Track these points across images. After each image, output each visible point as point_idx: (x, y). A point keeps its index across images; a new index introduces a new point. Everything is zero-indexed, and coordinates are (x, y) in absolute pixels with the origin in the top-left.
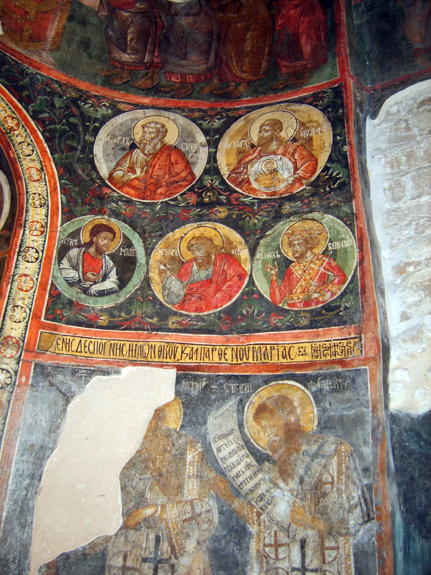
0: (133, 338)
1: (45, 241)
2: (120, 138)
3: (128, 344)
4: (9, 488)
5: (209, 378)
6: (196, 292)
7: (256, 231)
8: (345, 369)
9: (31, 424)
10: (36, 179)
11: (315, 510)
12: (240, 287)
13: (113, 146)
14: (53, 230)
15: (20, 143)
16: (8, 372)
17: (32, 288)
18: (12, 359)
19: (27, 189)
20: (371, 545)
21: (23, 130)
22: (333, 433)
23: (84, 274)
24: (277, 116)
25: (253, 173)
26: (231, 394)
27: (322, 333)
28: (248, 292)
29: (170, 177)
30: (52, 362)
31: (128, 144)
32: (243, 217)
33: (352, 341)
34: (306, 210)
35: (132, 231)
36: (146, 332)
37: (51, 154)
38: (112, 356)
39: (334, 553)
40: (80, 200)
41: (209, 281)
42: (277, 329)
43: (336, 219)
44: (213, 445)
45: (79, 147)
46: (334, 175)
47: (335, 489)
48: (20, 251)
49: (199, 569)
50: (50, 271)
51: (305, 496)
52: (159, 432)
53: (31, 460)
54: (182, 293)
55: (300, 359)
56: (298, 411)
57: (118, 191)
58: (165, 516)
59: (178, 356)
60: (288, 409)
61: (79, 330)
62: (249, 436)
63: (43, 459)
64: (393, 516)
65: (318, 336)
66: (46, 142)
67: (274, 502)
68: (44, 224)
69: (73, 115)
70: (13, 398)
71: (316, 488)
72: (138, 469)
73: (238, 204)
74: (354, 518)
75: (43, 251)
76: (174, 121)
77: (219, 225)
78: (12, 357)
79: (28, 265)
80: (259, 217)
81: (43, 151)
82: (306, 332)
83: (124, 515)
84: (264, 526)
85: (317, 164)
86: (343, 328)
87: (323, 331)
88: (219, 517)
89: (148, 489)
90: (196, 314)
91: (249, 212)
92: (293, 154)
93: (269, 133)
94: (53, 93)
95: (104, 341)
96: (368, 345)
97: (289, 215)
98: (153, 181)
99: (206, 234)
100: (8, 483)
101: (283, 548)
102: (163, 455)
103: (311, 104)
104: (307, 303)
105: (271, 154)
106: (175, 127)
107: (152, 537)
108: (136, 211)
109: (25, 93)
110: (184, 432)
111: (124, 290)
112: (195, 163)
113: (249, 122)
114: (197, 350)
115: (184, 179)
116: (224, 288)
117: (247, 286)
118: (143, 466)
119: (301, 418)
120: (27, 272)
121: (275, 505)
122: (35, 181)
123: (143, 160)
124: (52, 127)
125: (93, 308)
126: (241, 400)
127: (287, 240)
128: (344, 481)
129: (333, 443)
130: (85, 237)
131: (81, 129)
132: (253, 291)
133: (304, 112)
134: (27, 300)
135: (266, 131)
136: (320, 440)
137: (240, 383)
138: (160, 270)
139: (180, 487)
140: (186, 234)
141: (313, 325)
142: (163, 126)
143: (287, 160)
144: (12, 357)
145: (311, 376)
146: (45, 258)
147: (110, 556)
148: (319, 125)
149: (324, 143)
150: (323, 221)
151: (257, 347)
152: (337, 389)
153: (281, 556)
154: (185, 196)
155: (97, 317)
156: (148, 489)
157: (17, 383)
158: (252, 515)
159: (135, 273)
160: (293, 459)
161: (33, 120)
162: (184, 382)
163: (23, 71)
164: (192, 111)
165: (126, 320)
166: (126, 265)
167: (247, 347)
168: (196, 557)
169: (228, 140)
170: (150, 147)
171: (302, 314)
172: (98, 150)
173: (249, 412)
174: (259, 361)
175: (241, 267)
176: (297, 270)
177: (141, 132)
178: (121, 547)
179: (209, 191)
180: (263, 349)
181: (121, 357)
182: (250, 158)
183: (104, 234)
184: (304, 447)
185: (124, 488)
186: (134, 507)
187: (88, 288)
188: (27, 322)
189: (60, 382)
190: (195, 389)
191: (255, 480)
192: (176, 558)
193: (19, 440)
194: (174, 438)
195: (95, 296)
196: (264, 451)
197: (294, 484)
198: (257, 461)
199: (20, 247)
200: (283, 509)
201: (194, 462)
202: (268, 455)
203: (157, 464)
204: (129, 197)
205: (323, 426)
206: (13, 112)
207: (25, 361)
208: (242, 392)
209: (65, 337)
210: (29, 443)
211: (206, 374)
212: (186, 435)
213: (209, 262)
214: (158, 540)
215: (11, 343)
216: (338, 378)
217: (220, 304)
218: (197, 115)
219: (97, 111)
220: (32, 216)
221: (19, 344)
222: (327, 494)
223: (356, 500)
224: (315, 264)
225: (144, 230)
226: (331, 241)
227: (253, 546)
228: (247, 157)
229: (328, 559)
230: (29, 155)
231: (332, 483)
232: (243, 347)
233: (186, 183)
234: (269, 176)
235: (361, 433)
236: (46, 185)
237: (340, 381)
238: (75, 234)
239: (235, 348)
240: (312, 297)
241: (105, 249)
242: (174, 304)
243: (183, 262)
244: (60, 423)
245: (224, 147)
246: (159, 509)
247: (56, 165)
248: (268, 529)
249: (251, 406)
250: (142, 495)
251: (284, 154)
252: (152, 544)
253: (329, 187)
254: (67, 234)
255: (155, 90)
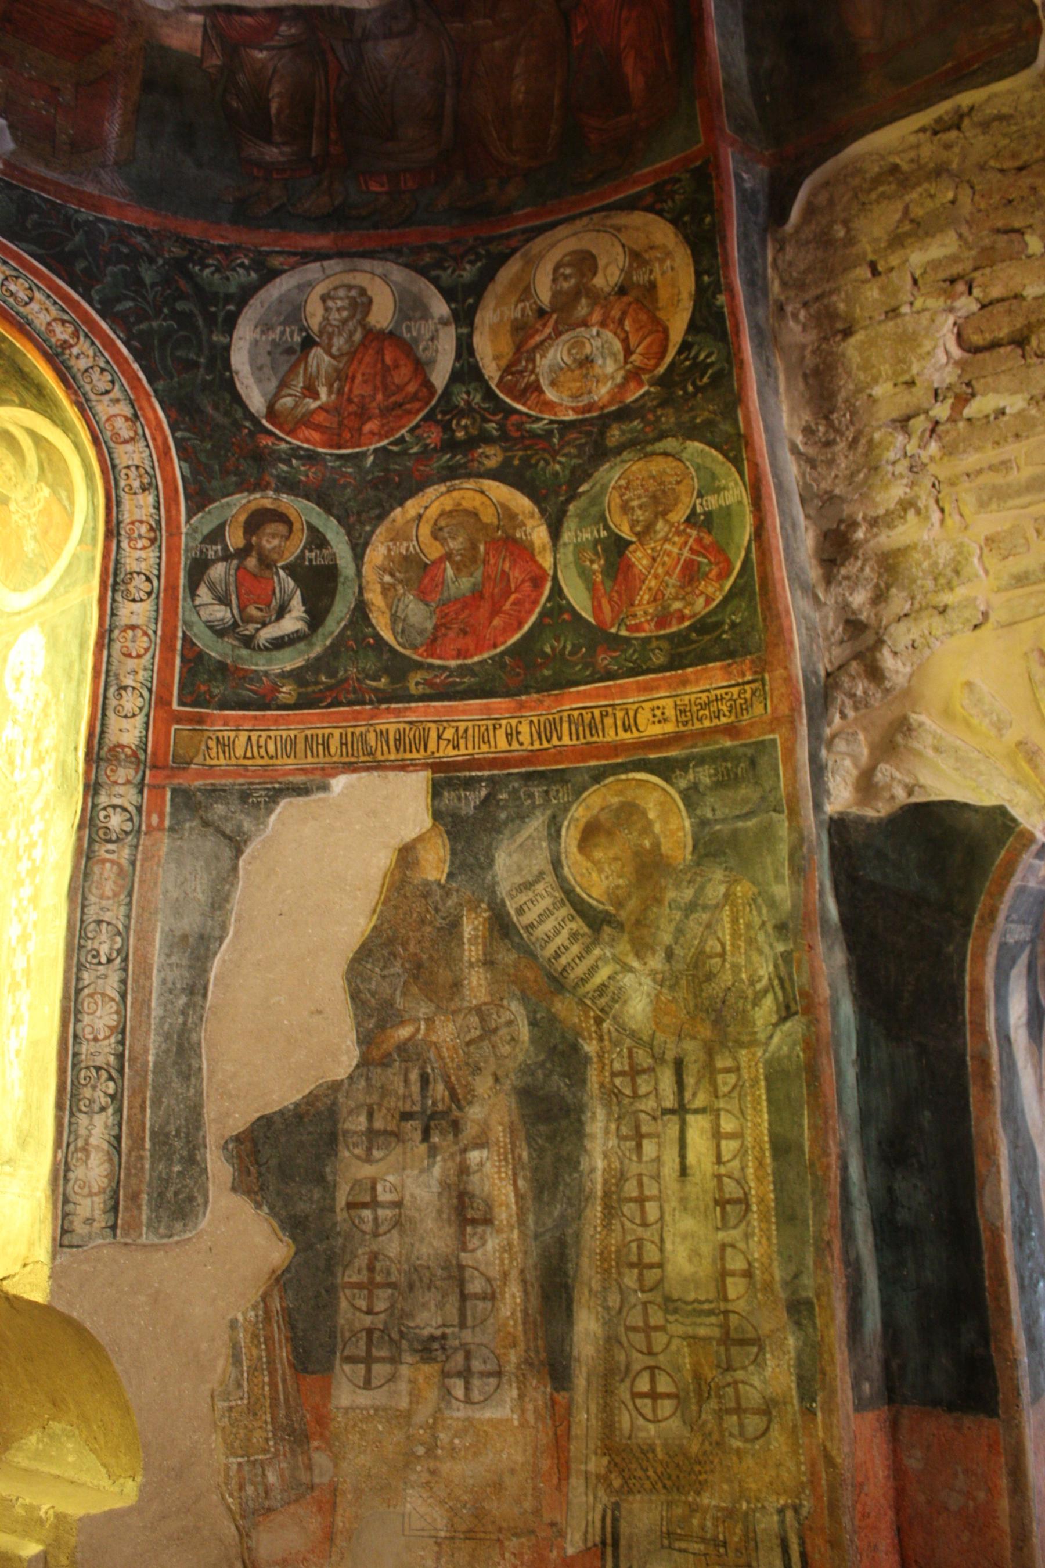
0: (345, 720)
1: (160, 558)
2: (279, 329)
3: (337, 732)
4: (153, 1014)
5: (492, 780)
6: (455, 620)
7: (560, 487)
8: (736, 743)
9: (177, 900)
10: (127, 437)
11: (696, 1006)
12: (535, 602)
13: (269, 348)
14: (174, 532)
15: (86, 371)
16: (125, 810)
17: (147, 650)
18: (128, 787)
19: (112, 459)
20: (794, 1059)
21: (88, 343)
22: (720, 864)
23: (242, 609)
24: (586, 242)
25: (546, 369)
26: (534, 807)
27: (692, 677)
28: (552, 608)
29: (387, 397)
30: (201, 782)
31: (297, 339)
32: (533, 461)
33: (747, 687)
34: (651, 435)
35: (324, 515)
36: (368, 707)
37: (150, 382)
38: (310, 759)
39: (732, 1079)
40: (217, 467)
41: (477, 595)
42: (610, 676)
43: (707, 448)
44: (508, 903)
45: (202, 360)
46: (702, 357)
47: (728, 966)
48: (116, 583)
49: (501, 1124)
50: (177, 614)
51: (677, 983)
52: (408, 890)
53: (185, 962)
54: (429, 625)
55: (657, 730)
56: (657, 828)
57: (288, 439)
58: (434, 1038)
59: (432, 746)
60: (639, 826)
61: (244, 717)
62: (573, 882)
63: (207, 957)
64: (834, 1006)
65: (684, 683)
66: (137, 359)
67: (623, 998)
68: (153, 524)
69: (182, 296)
70: (139, 857)
71: (696, 967)
72: (378, 960)
73: (523, 437)
74: (766, 1011)
75: (158, 577)
76: (384, 278)
77: (488, 484)
78: (128, 782)
79: (135, 607)
80: (563, 459)
81: (133, 379)
82: (664, 678)
83: (360, 1043)
84: (610, 1040)
85: (667, 338)
86: (730, 665)
87: (695, 673)
88: (530, 1032)
89: (398, 993)
90: (459, 662)
91: (544, 450)
92: (621, 322)
93: (573, 281)
94: (135, 257)
95: (292, 733)
96: (776, 693)
97: (619, 450)
98: (353, 408)
99: (466, 504)
100: (149, 1006)
101: (645, 1077)
102: (419, 930)
103: (650, 209)
104: (662, 621)
105: (579, 326)
106: (383, 290)
107: (414, 1076)
108: (328, 474)
109: (80, 265)
110: (454, 885)
111: (320, 631)
112: (432, 362)
113: (532, 263)
114: (466, 731)
115: (415, 397)
116: (507, 606)
117: (549, 600)
118: (385, 952)
119: (662, 840)
120: (134, 620)
121: (625, 1002)
122: (126, 442)
123: (330, 370)
124: (144, 326)
125: (266, 674)
126: (554, 817)
127: (618, 500)
128: (743, 950)
129: (722, 882)
130: (235, 539)
131: (200, 322)
132: (560, 607)
133: (637, 229)
134: (141, 673)
135: (566, 278)
136: (699, 879)
137: (549, 785)
138: (383, 584)
139: (456, 985)
140: (426, 508)
141: (675, 663)
142: (363, 291)
143: (610, 335)
144: (128, 782)
145: (676, 760)
146: (165, 590)
147: (344, 1112)
148: (668, 254)
149: (679, 293)
150: (684, 456)
151: (576, 713)
152: (724, 782)
153: (643, 1090)
154: (419, 432)
155: (276, 689)
156: (398, 993)
157: (144, 828)
158: (587, 1022)
159: (338, 598)
160: (652, 917)
161: (104, 318)
162: (446, 794)
163: (68, 219)
164: (417, 251)
165: (330, 688)
166: (319, 583)
167: (557, 717)
168: (494, 1105)
169: (492, 305)
170: (342, 341)
171: (654, 644)
172: (240, 359)
173: (570, 837)
174: (583, 741)
175: (535, 562)
176: (639, 558)
177: (320, 312)
178: (361, 1097)
179: (463, 417)
180: (587, 717)
181: (328, 759)
182: (538, 338)
183: (272, 528)
184: (671, 894)
185: (355, 996)
186: (377, 1026)
187: (252, 637)
188: (148, 715)
189: (220, 817)
190: (467, 804)
191: (589, 961)
192: (460, 1108)
193: (159, 930)
194: (438, 898)
195: (267, 649)
196: (601, 907)
197: (656, 962)
198: (590, 926)
199: (116, 575)
200: (639, 1007)
201: (477, 937)
202: (607, 912)
203: (412, 948)
204: (311, 447)
205: (702, 851)
206: (63, 310)
207: (152, 787)
208: (554, 801)
209: (220, 734)
210: (178, 933)
211: (486, 773)
212: (457, 891)
213: (474, 560)
214: (425, 1080)
215: (123, 756)
216: (726, 761)
217: (501, 639)
218: (427, 258)
219: (228, 279)
220: (131, 512)
221: (137, 757)
222: (715, 976)
223: (765, 982)
224: (674, 543)
225: (346, 511)
226: (700, 495)
227: (593, 1077)
228: (532, 336)
229: (724, 1089)
230: (107, 392)
231: (722, 955)
232: (550, 717)
233: (417, 405)
234: (577, 372)
235: (769, 860)
236: (148, 446)
237: (729, 765)
238: (216, 535)
239: (535, 720)
240: (672, 609)
241: (275, 556)
242: (415, 648)
243: (426, 565)
244: (229, 891)
245: (487, 322)
246: (423, 1027)
247: (161, 403)
248: (616, 1046)
249: (572, 827)
250: (390, 1004)
251: (603, 324)
252: (415, 1088)
253: (694, 384)
254: (199, 537)
255: (337, 218)
